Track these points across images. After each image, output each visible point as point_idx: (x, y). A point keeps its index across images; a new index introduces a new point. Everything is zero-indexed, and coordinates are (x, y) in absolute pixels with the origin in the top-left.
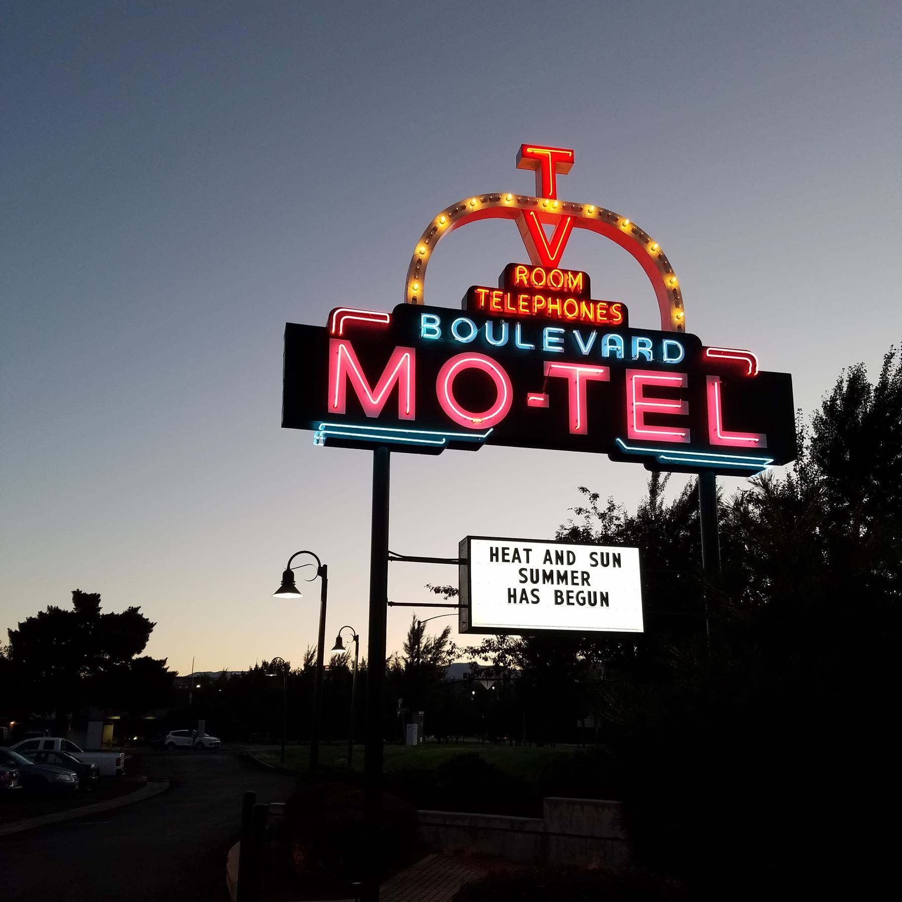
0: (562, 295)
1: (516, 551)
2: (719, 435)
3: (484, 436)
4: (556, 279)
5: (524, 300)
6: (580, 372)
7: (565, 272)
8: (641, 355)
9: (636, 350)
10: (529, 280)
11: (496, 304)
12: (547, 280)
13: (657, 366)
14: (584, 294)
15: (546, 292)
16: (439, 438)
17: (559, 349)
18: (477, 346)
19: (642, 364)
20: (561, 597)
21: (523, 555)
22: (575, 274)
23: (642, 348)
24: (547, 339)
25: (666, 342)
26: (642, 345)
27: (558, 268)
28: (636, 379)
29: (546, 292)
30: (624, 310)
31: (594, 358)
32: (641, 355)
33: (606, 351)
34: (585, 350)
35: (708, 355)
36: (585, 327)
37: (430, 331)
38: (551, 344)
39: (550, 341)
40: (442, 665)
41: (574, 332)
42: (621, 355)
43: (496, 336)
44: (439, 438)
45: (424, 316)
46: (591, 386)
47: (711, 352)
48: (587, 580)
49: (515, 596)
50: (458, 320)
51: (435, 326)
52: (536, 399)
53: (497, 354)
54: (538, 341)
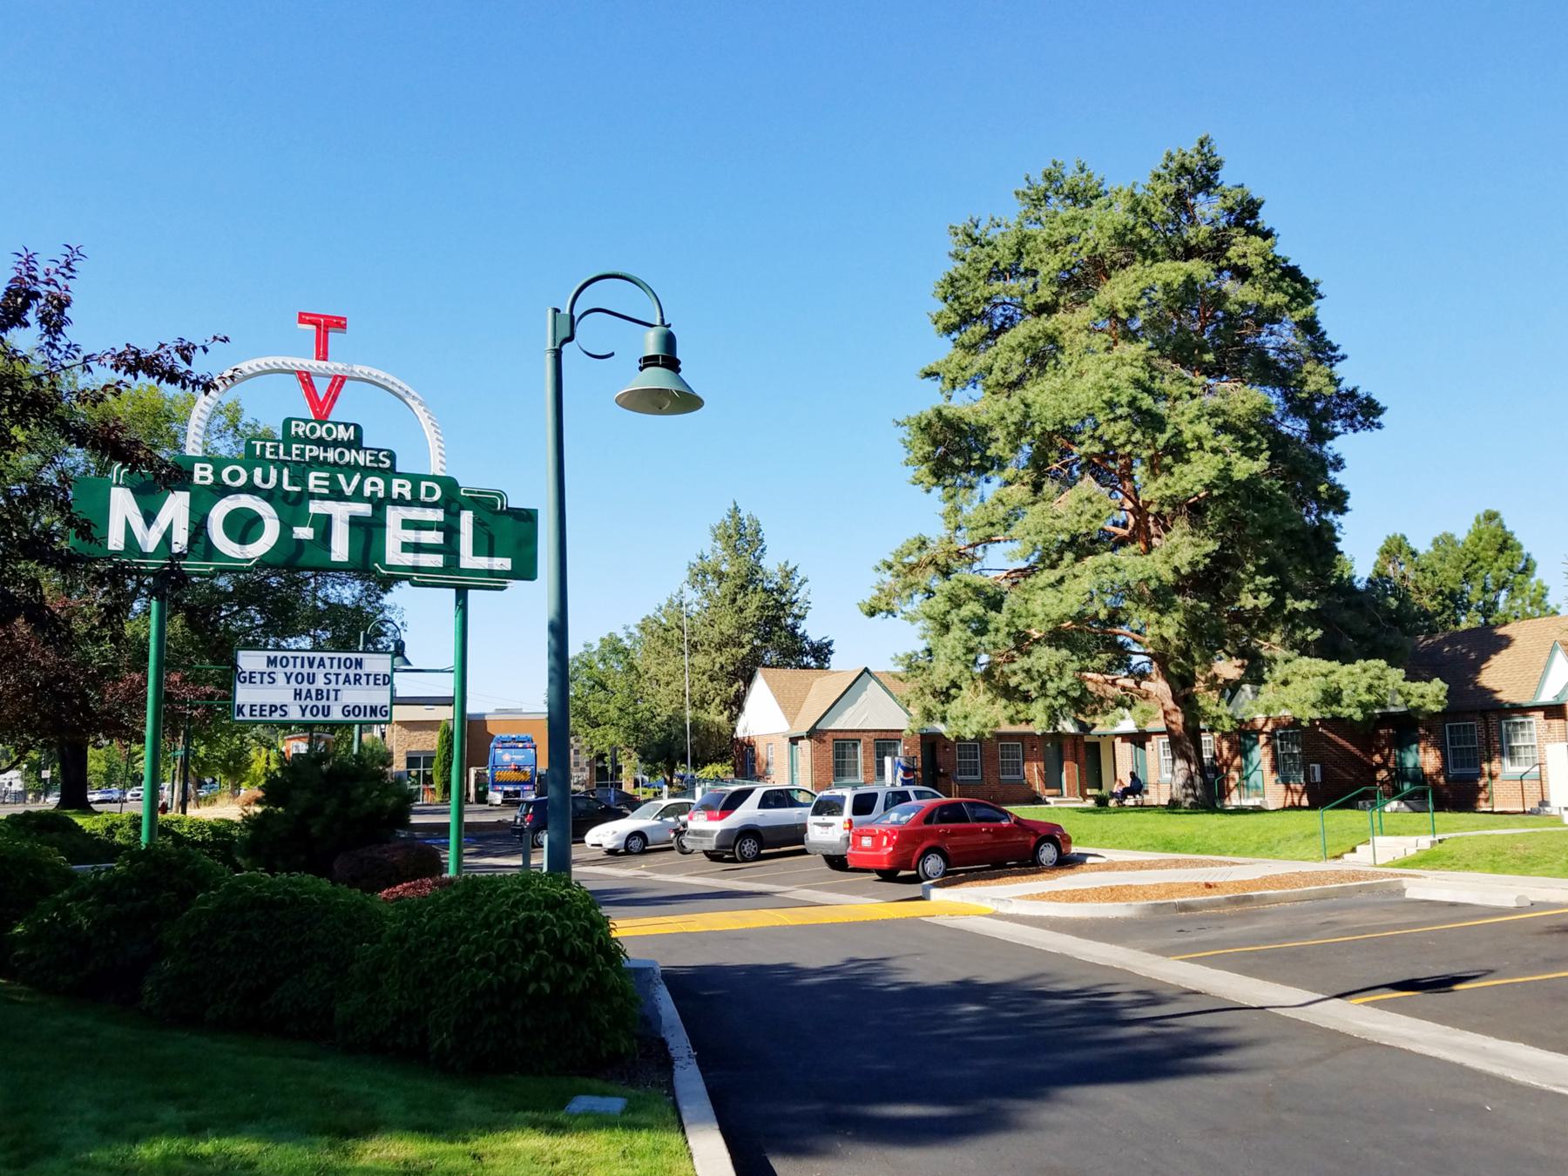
0: (336, 443)
1: (322, 659)
2: (468, 560)
3: (383, 571)
4: (329, 431)
5: (297, 449)
6: (341, 513)
7: (336, 424)
8: (400, 494)
9: (395, 491)
10: (304, 432)
11: (271, 453)
12: (321, 432)
13: (415, 502)
14: (356, 444)
15: (320, 442)
16: (208, 566)
17: (326, 491)
18: (250, 489)
19: (401, 501)
20: (321, 694)
21: (327, 662)
22: (347, 426)
23: (401, 488)
24: (312, 482)
25: (424, 484)
26: (401, 486)
27: (329, 419)
28: (394, 515)
29: (320, 442)
30: (392, 456)
31: (358, 496)
32: (400, 494)
33: (367, 491)
34: (348, 491)
35: (462, 493)
36: (352, 468)
37: (203, 478)
38: (316, 486)
39: (314, 480)
40: (1302, 781)
41: (339, 475)
42: (381, 495)
43: (265, 480)
44: (208, 566)
45: (197, 466)
46: (355, 522)
47: (465, 491)
48: (359, 680)
49: (300, 694)
50: (230, 469)
51: (208, 473)
52: (304, 533)
53: (269, 496)
54: (305, 484)
